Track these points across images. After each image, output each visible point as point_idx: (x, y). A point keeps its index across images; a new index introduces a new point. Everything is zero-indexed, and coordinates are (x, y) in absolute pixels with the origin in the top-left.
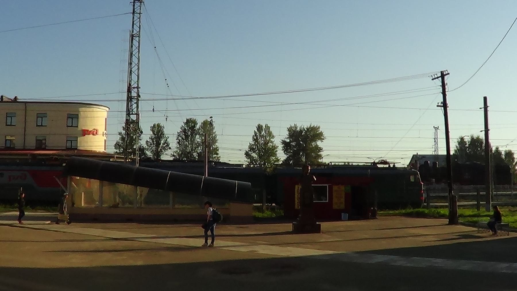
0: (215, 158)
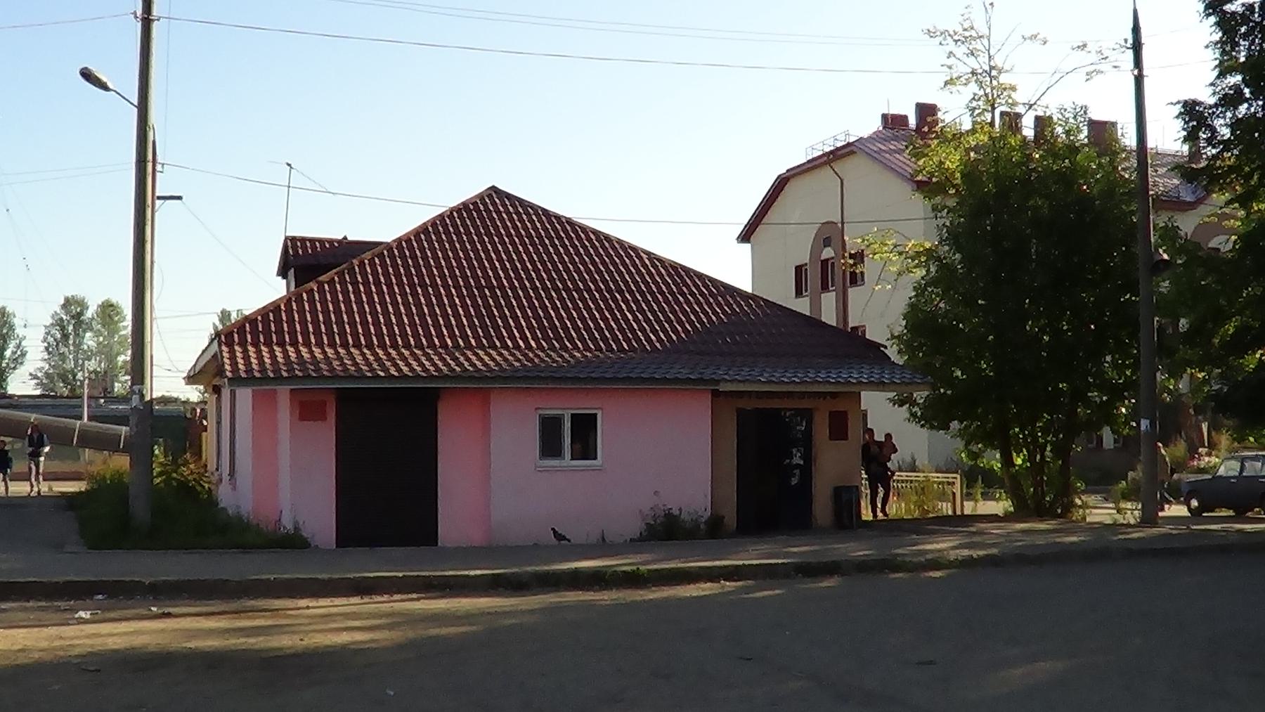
0: (1220, 167)
